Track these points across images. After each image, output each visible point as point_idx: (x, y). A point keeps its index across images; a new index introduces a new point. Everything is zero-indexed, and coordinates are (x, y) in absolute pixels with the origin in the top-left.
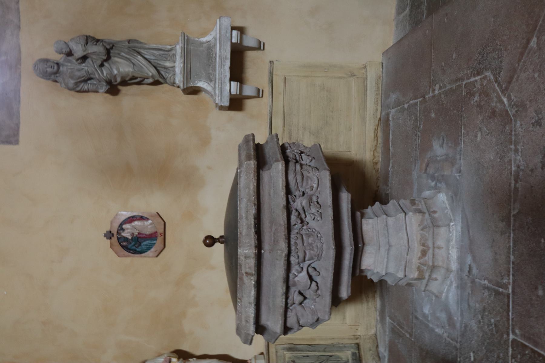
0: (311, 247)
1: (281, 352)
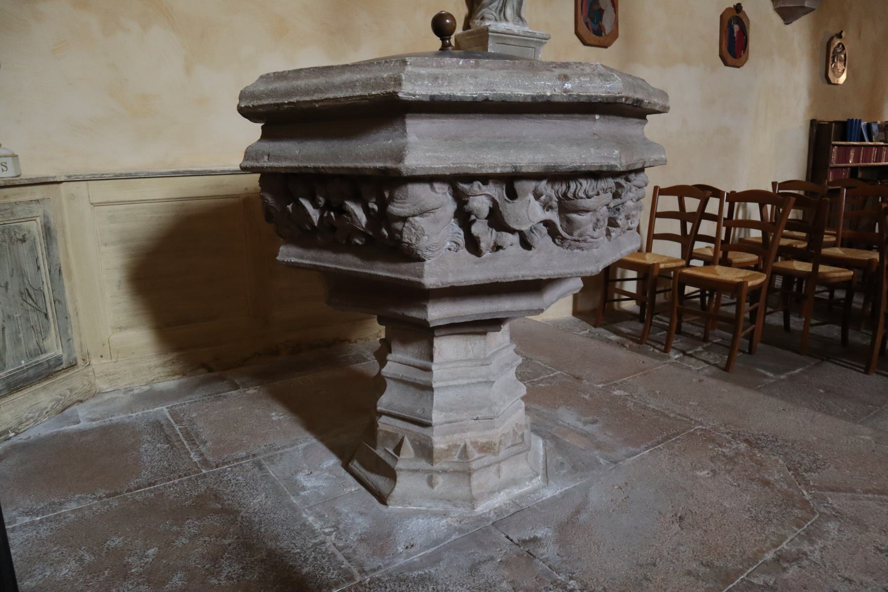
1: (38, 210)
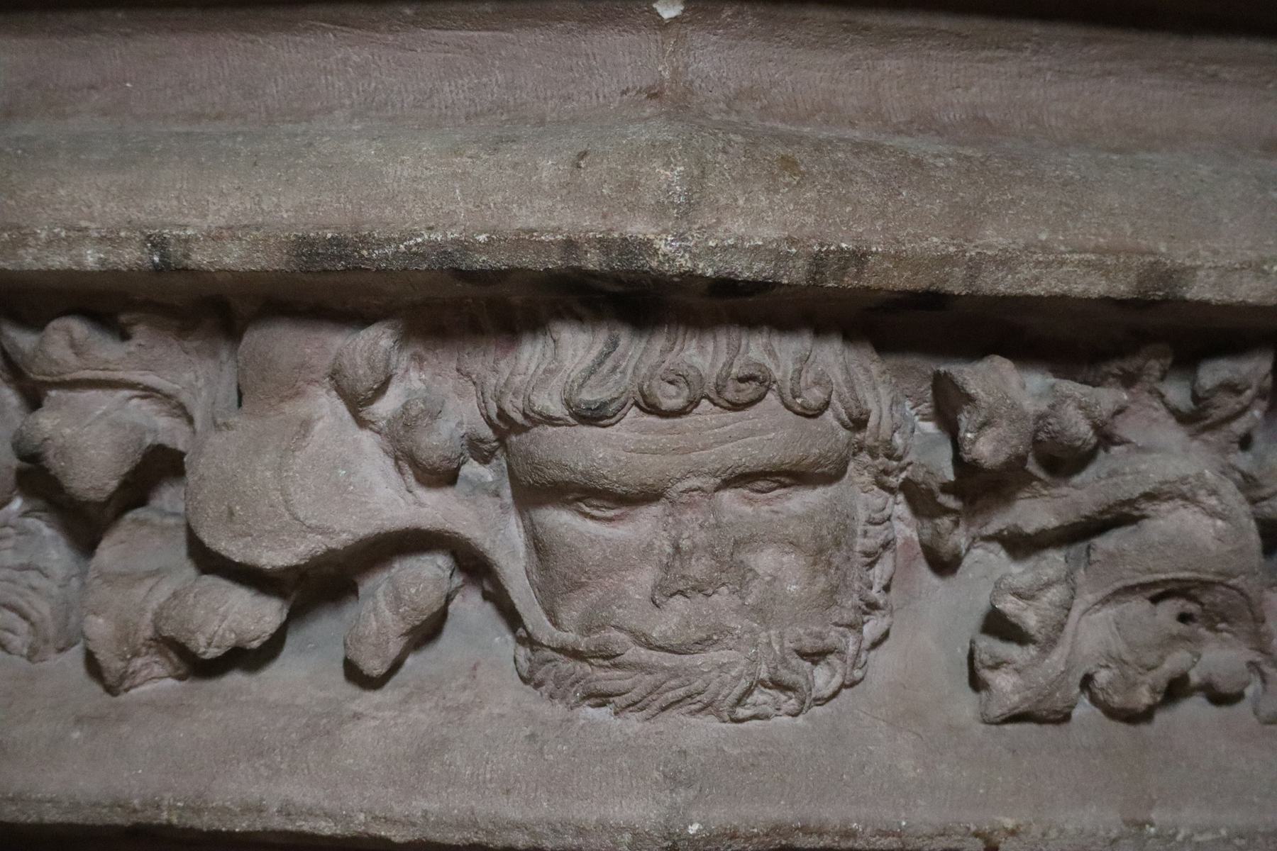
0: (699, 568)
